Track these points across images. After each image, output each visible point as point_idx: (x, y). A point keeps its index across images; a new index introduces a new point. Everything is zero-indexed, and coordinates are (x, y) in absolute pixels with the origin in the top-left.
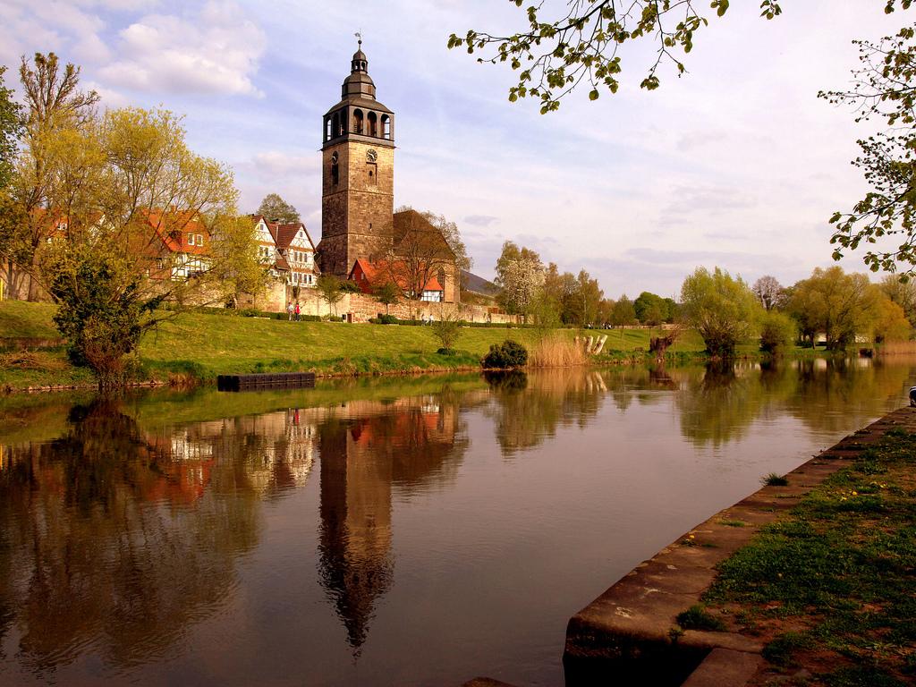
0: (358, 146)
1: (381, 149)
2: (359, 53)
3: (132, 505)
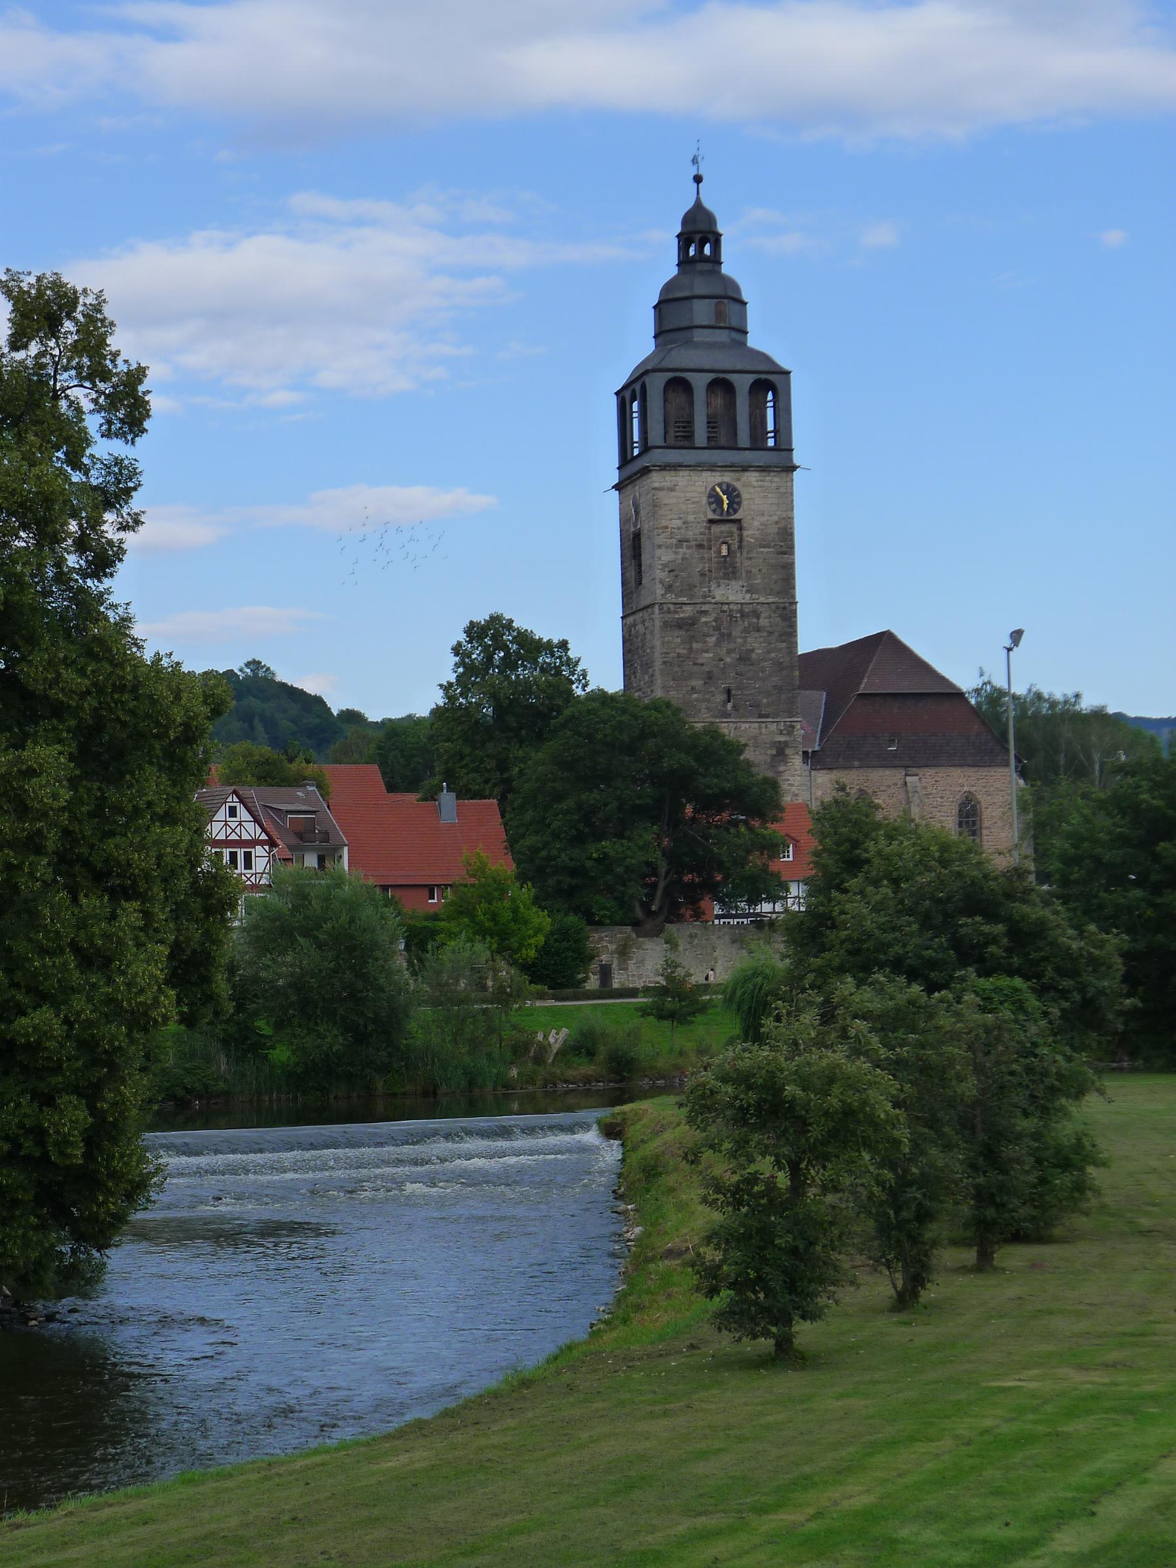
0: (682, 479)
1: (752, 477)
2: (698, 208)
3: (223, 1059)
